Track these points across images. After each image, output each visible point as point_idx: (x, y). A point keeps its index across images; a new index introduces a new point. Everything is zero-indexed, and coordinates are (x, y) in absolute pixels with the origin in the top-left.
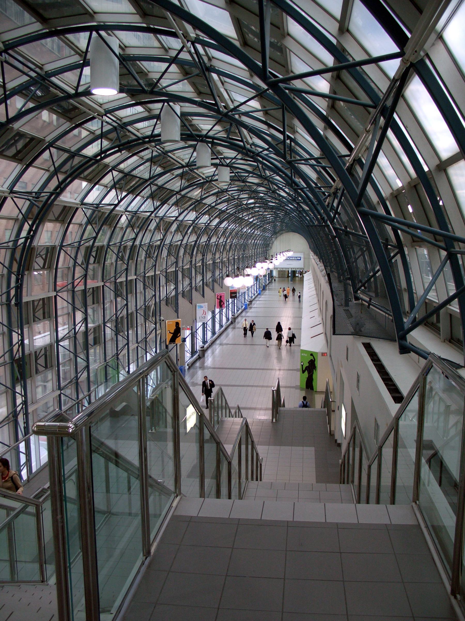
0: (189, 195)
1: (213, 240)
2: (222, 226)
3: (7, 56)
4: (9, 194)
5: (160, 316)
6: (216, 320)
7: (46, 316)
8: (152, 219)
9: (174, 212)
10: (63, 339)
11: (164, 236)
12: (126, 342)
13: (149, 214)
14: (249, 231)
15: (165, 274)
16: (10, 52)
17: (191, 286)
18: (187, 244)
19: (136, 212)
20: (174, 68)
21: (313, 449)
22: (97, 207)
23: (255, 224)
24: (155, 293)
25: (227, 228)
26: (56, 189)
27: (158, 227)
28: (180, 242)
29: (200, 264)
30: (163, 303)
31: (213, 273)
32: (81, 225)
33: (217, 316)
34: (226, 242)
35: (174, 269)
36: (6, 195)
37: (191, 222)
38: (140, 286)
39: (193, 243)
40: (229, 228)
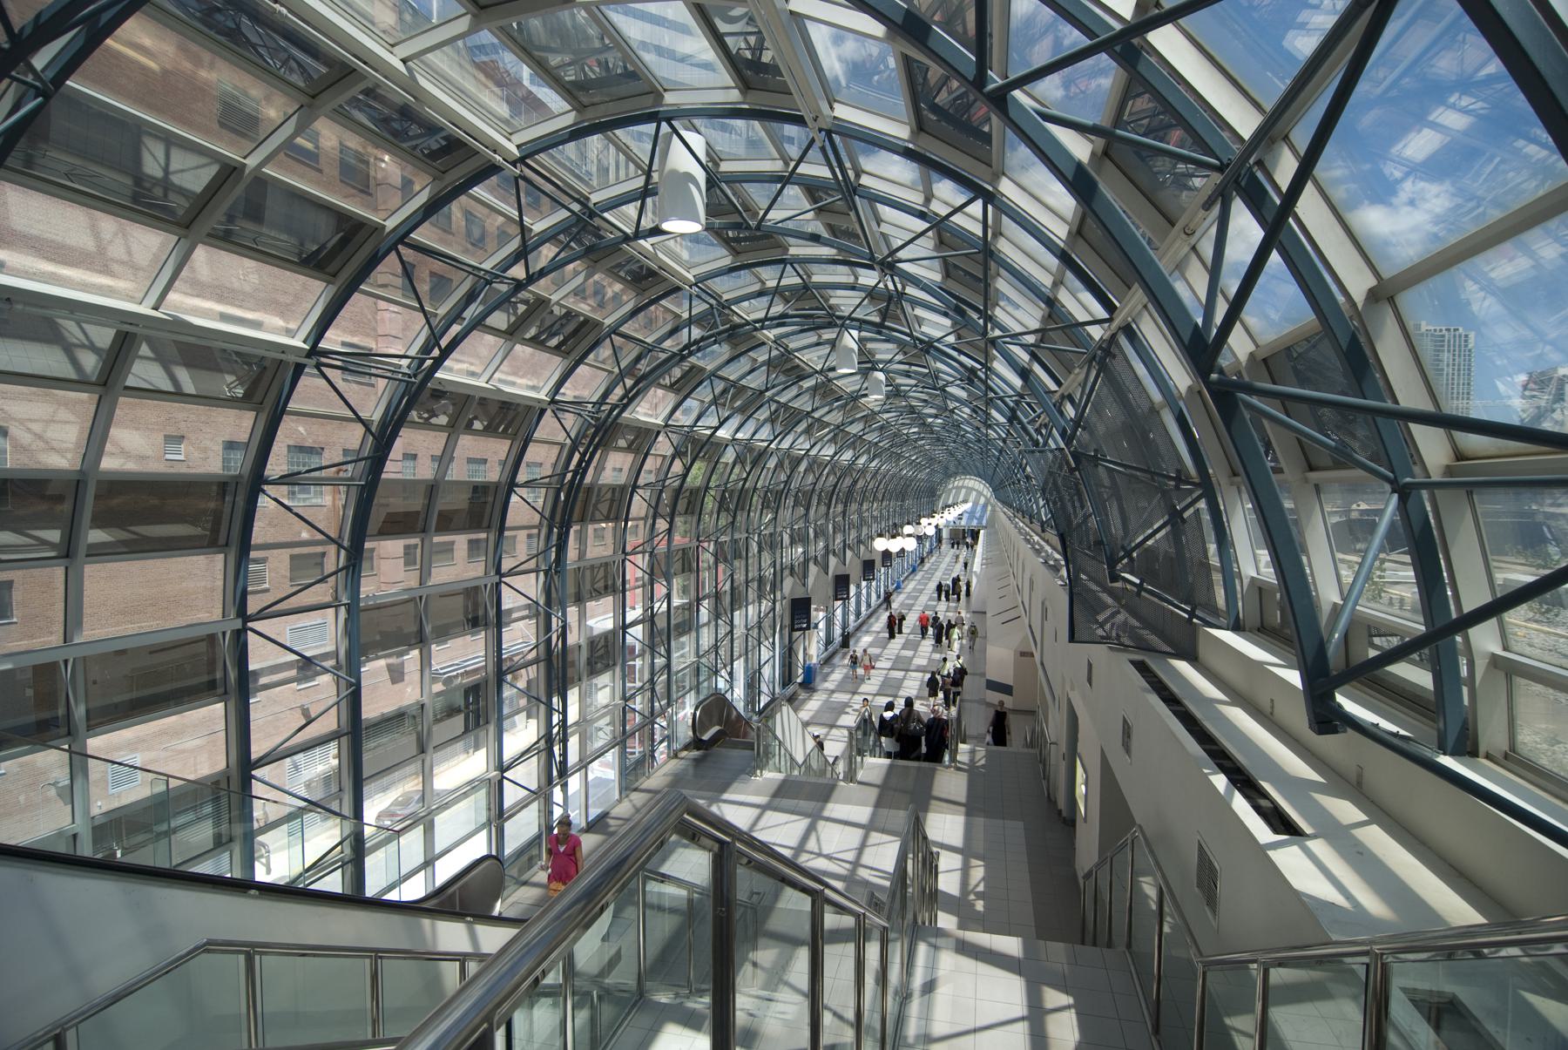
0: (825, 419)
3: (524, 168)
7: (609, 589)
9: (803, 444)
10: (634, 624)
12: (728, 628)
13: (766, 444)
16: (529, 161)
20: (793, 191)
21: (1020, 824)
25: (879, 469)
26: (621, 399)
27: (780, 465)
30: (786, 572)
32: (664, 457)
33: (864, 592)
36: (544, 406)
37: (828, 458)
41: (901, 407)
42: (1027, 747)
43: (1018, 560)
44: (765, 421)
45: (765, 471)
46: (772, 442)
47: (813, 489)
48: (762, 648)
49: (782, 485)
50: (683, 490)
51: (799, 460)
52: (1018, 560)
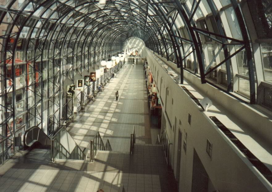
1: (95, 40)
2: (100, 32)
4: (8, 11)
5: (60, 86)
6: (95, 84)
8: (58, 25)
11: (66, 35)
13: (55, 21)
14: (114, 36)
15: (66, 58)
17: (82, 53)
18: (79, 41)
19: (21, 12)
21: (158, 176)
22: (47, 20)
23: (118, 32)
24: (60, 69)
25: (102, 33)
27: (61, 30)
28: (75, 40)
29: (87, 53)
31: (94, 58)
34: (101, 41)
35: (72, 56)
38: (51, 63)
39: (83, 41)
40: (104, 33)
41: (112, 8)
42: (159, 144)
43: (155, 70)
44: (55, 11)
45: (56, 32)
46: (58, 20)
47: (76, 41)
48: (55, 105)
49: (63, 39)
50: (19, 39)
51: (70, 29)
52: (155, 70)
